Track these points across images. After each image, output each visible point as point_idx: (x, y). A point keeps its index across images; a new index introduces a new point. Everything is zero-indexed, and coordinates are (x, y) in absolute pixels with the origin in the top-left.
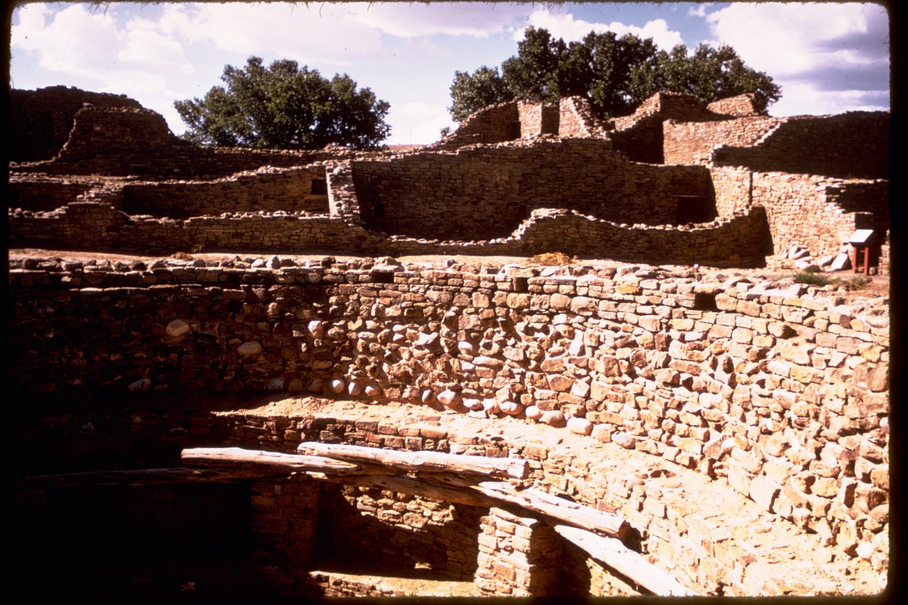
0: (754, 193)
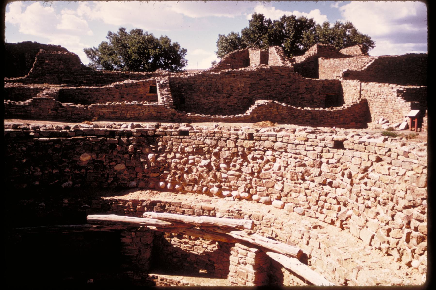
0: (362, 92)
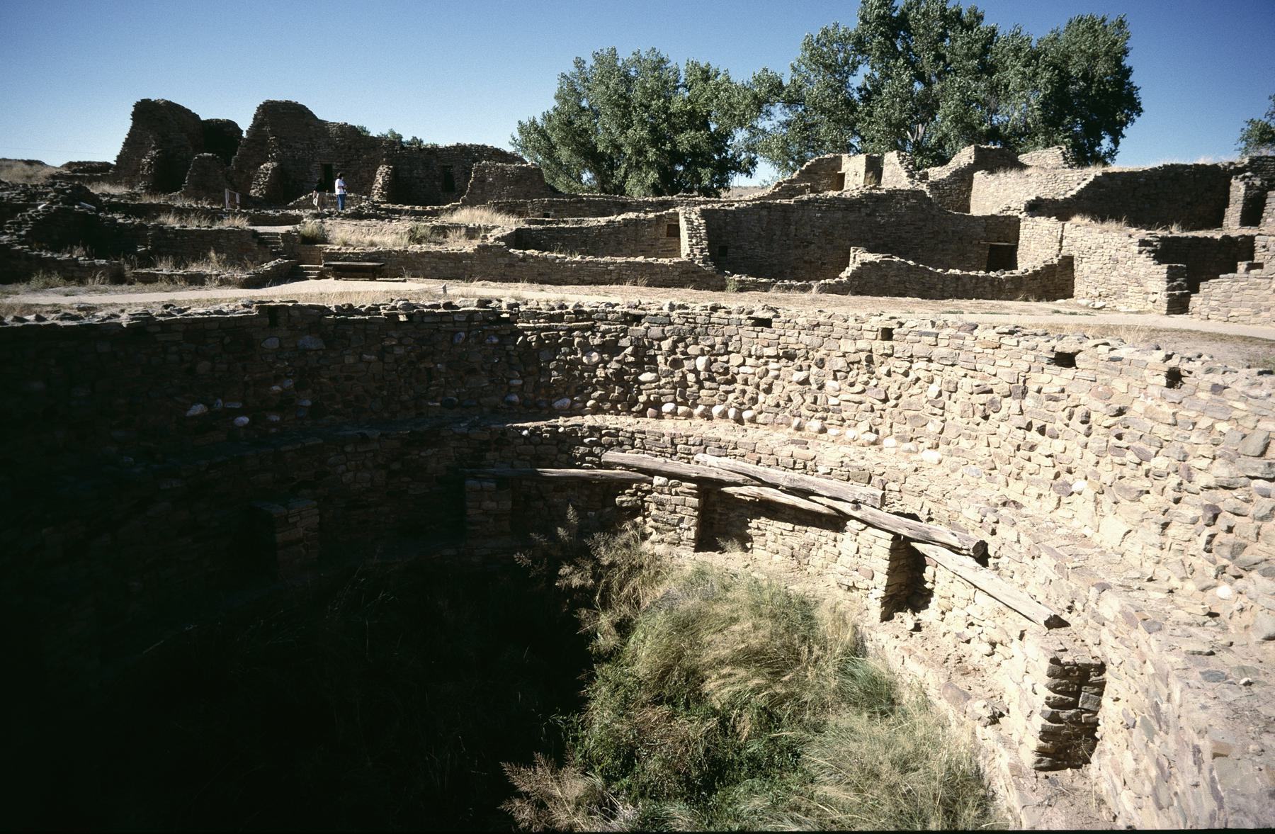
0: (1064, 243)
